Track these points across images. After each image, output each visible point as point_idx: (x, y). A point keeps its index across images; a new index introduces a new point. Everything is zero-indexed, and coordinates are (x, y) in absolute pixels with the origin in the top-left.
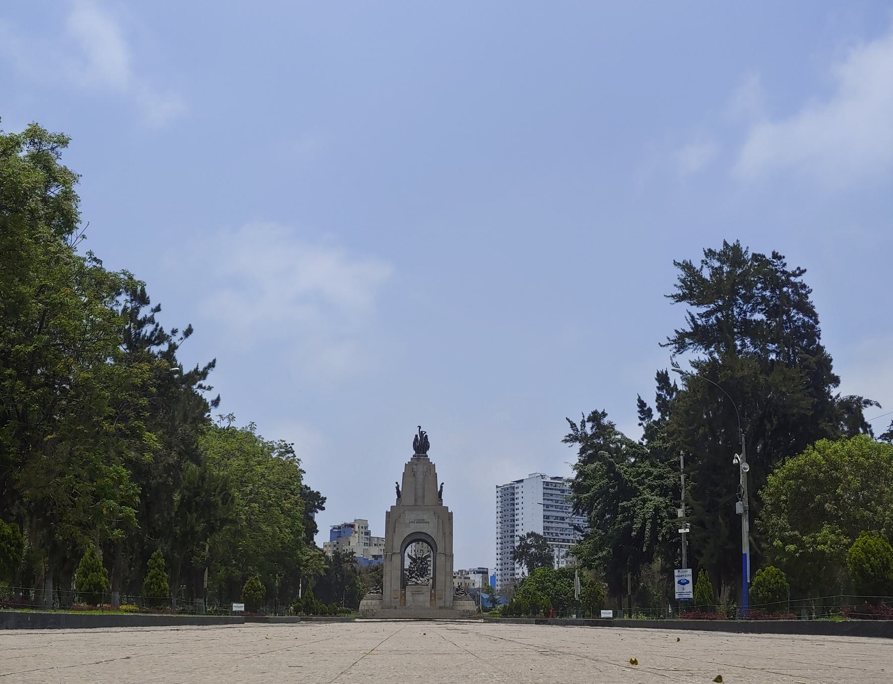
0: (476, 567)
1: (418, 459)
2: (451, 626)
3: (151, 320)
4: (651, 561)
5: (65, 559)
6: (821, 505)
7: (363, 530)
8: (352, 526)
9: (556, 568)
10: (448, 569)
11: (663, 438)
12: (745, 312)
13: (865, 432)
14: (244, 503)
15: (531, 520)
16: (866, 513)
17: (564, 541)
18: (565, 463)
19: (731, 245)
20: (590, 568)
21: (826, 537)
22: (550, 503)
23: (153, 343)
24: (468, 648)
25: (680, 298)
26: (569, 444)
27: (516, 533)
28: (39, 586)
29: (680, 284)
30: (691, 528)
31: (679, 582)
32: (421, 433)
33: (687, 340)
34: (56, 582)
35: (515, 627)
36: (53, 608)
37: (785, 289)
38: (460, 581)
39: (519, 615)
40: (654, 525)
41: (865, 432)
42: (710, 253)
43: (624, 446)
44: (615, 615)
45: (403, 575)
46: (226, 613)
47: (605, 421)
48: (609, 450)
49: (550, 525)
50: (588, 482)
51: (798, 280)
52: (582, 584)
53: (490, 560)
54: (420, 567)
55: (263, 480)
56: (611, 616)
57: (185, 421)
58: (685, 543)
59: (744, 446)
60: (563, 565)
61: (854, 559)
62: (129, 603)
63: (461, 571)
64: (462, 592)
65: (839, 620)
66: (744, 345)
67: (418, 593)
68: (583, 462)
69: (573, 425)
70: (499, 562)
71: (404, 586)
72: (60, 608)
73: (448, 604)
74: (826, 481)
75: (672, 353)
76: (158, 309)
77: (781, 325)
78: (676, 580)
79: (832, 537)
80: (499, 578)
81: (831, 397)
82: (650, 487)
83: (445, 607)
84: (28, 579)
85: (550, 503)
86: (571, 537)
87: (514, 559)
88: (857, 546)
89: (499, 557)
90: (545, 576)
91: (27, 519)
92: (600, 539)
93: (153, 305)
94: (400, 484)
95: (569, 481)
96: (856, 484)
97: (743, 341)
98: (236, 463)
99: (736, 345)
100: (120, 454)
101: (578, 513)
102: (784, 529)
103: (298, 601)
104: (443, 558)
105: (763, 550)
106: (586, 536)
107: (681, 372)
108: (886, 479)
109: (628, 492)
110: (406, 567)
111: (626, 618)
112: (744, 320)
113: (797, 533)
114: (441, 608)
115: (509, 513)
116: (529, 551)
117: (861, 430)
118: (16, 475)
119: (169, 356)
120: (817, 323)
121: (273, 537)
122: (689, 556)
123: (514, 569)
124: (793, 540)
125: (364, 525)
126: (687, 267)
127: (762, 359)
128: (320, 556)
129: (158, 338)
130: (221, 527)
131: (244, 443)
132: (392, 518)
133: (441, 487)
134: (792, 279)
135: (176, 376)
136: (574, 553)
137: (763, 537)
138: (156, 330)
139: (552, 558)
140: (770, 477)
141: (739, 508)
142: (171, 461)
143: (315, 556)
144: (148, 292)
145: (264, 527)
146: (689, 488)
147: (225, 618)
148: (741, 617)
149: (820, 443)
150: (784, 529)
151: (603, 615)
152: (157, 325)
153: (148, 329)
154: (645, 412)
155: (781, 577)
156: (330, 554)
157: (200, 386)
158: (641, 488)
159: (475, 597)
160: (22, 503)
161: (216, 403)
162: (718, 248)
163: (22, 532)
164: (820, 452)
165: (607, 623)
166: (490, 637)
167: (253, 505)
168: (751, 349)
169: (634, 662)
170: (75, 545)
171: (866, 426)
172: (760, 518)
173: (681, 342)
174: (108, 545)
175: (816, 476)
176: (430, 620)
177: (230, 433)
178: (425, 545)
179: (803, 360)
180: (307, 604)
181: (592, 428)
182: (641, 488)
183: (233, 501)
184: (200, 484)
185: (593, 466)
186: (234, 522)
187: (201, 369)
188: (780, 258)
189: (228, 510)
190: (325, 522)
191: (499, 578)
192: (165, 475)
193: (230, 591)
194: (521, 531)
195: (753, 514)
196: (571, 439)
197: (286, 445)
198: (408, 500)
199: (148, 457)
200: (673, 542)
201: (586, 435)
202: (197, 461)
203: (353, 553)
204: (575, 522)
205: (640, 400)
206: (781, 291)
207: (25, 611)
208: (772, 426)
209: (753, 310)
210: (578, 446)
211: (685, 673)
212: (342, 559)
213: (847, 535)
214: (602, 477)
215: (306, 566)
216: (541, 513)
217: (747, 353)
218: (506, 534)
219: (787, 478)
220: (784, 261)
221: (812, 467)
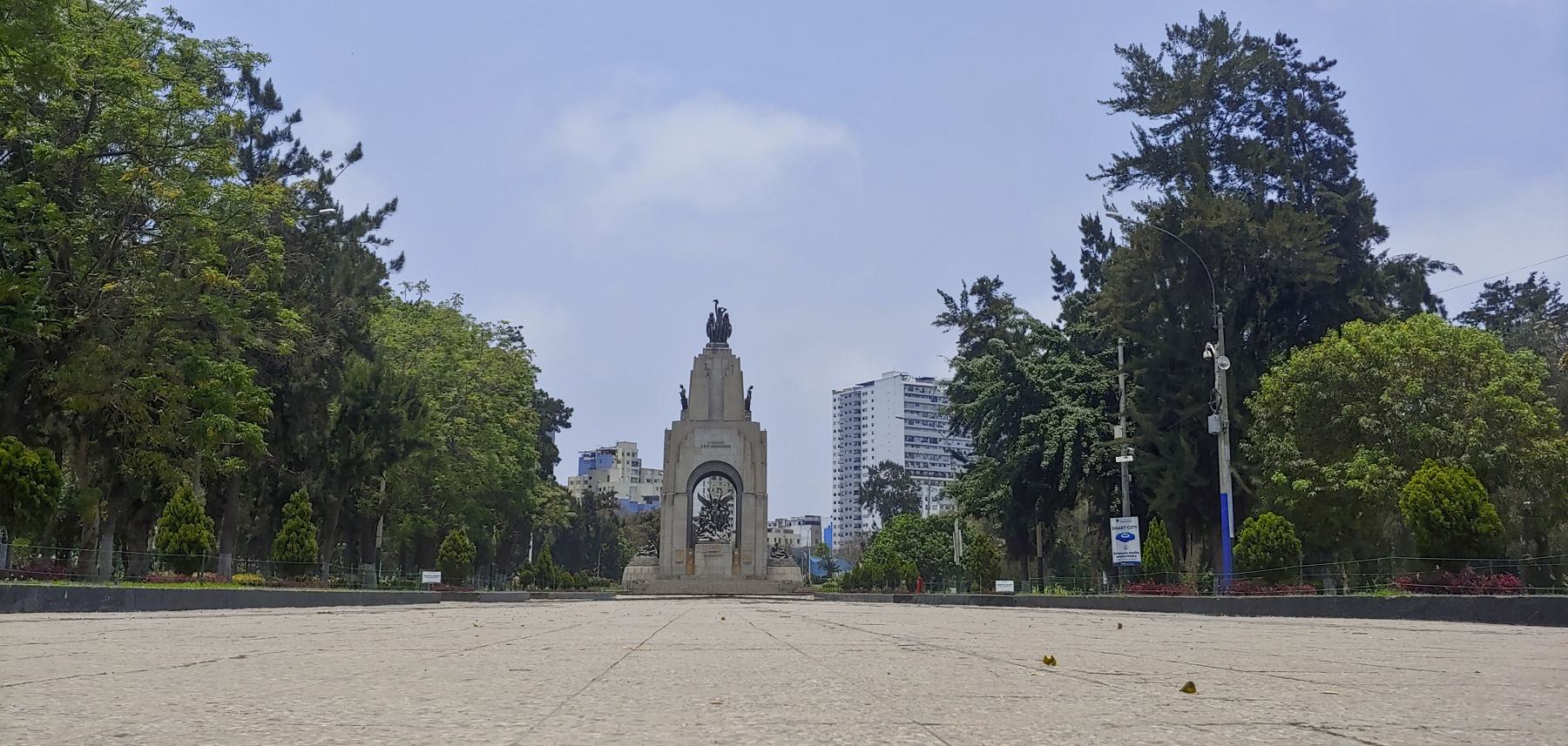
0: (802, 515)
2: (764, 605)
3: (287, 136)
4: (1072, 505)
5: (137, 505)
6: (1353, 418)
7: (630, 458)
8: (613, 452)
9: (925, 516)
10: (760, 518)
11: (1091, 319)
12: (1229, 126)
13: (1432, 309)
14: (444, 417)
15: (886, 443)
16: (1433, 430)
17: (936, 474)
18: (939, 358)
19: (1210, 18)
20: (978, 515)
21: (1361, 469)
22: (915, 416)
24: (790, 640)
25: (1123, 106)
26: (943, 328)
27: (863, 463)
28: (89, 545)
29: (1126, 82)
30: (1136, 455)
31: (1119, 537)
32: (719, 311)
34: (121, 539)
35: (864, 607)
36: (112, 579)
37: (1297, 92)
38: (778, 536)
39: (869, 589)
41: (1432, 309)
42: (1177, 32)
43: (1029, 331)
44: (1018, 588)
45: (690, 527)
46: (411, 586)
47: (999, 293)
48: (1004, 336)
49: (914, 450)
50: (974, 385)
51: (1320, 77)
52: (966, 540)
54: (716, 514)
55: (474, 382)
56: (1012, 589)
57: (348, 292)
58: (1126, 478)
59: (1221, 331)
60: (935, 512)
61: (1414, 501)
62: (248, 570)
63: (780, 521)
64: (779, 553)
65: (1390, 595)
66: (1225, 178)
67: (713, 554)
68: (965, 355)
69: (948, 300)
70: (838, 506)
71: (692, 544)
72: (125, 580)
73: (759, 573)
74: (1366, 384)
75: (1107, 189)
76: (296, 118)
77: (1289, 148)
78: (1114, 534)
79: (1374, 468)
80: (837, 531)
81: (1371, 257)
82: (1069, 392)
84: (69, 533)
85: (915, 416)
86: (948, 469)
87: (861, 502)
89: (838, 498)
90: (908, 528)
91: (70, 440)
92: (993, 472)
93: (288, 111)
94: (687, 388)
95: (943, 383)
96: (1416, 387)
97: (1224, 170)
98: (429, 356)
99: (1211, 178)
100: (239, 341)
101: (957, 432)
102: (1290, 457)
103: (528, 567)
104: (752, 500)
105: (1254, 488)
106: (971, 467)
107: (1119, 219)
108: (1469, 380)
110: (696, 514)
111: (1035, 592)
112: (1228, 138)
113: (1311, 461)
114: (748, 577)
115: (853, 432)
116: (886, 491)
117: (1424, 307)
118: (49, 374)
119: (319, 194)
120: (1352, 144)
121: (489, 468)
122: (1132, 498)
123: (860, 518)
124: (1305, 472)
126: (1136, 55)
127: (1253, 199)
128: (563, 498)
129: (298, 163)
130: (405, 454)
131: (443, 326)
132: (674, 441)
134: (1311, 75)
136: (954, 494)
137: (1254, 468)
138: (295, 151)
139: (919, 500)
140: (1264, 378)
141: (1214, 424)
142: (324, 353)
144: (279, 92)
145: (475, 454)
146: (1132, 394)
147: (406, 592)
148: (1222, 591)
149: (1351, 327)
150: (1290, 457)
151: (998, 589)
152: (297, 144)
153: (281, 150)
154: (1062, 278)
155: (1286, 529)
156: (578, 495)
157: (371, 239)
158: (1055, 394)
159: (800, 561)
160: (60, 417)
161: (398, 264)
162: (1191, 23)
163: (59, 460)
164: (1350, 341)
165: (1006, 601)
166: (823, 623)
168: (1238, 183)
169: (1050, 661)
170: (156, 482)
171: (1433, 302)
172: (1248, 440)
173: (1121, 173)
174: (216, 485)
175: (1344, 377)
176: (731, 596)
177: (421, 311)
178: (725, 480)
180: (542, 572)
181: (979, 303)
182: (1055, 394)
183: (424, 413)
184: (373, 387)
185: (981, 361)
186: (424, 446)
187: (372, 214)
188: (1289, 43)
189: (418, 428)
190: (570, 445)
191: (837, 531)
192: (315, 375)
193: (418, 553)
194: (871, 460)
195: (1236, 434)
196: (947, 320)
197: (510, 329)
198: (699, 412)
199: (286, 346)
200: (1107, 475)
201: (970, 314)
202: (368, 353)
203: (613, 493)
204: (954, 445)
205: (1054, 260)
206: (1290, 94)
207: (59, 584)
208: (1268, 300)
209: (1243, 123)
210: (957, 331)
211: (1134, 679)
213: (1398, 465)
214: (994, 378)
215: (540, 514)
216: (902, 433)
217: (1232, 190)
218: (848, 464)
219: (1293, 379)
220: (1297, 46)
221: (1336, 362)
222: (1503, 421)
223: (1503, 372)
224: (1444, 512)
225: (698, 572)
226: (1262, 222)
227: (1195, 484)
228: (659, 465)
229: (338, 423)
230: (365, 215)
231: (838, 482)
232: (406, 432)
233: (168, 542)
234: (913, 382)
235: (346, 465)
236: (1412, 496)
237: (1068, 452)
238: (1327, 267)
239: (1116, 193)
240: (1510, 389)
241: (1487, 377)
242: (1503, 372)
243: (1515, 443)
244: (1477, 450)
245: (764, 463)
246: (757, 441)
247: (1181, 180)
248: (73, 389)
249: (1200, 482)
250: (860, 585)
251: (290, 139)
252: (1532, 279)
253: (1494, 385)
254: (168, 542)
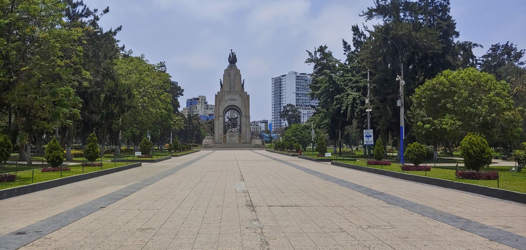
0: (261, 120)
1: (231, 67)
6: (445, 104)
8: (198, 99)
15: (290, 98)
17: (306, 106)
22: (299, 86)
23: (84, 16)
26: (308, 64)
27: (282, 105)
30: (373, 109)
31: (366, 136)
32: (232, 53)
33: (374, 13)
40: (353, 107)
47: (327, 51)
49: (299, 98)
53: (269, 117)
54: (233, 123)
58: (369, 117)
61: (464, 147)
63: (254, 122)
64: (256, 134)
66: (405, 15)
67: (233, 136)
69: (310, 54)
70: (273, 117)
71: (225, 132)
78: (365, 135)
80: (273, 125)
81: (454, 43)
82: (351, 87)
83: (246, 143)
85: (299, 86)
88: (465, 141)
89: (273, 114)
90: (297, 129)
92: (325, 114)
98: (134, 77)
99: (400, 16)
102: (424, 116)
104: (245, 118)
105: (412, 123)
109: (339, 90)
113: (431, 118)
116: (289, 114)
119: (94, 23)
120: (449, 4)
121: (156, 114)
122: (371, 122)
124: (428, 122)
125: (204, 98)
132: (218, 97)
135: (99, 34)
138: (85, 9)
139: (300, 116)
141: (399, 103)
143: (178, 119)
146: (372, 87)
149: (445, 72)
150: (424, 116)
152: (85, 6)
153: (80, 9)
158: (346, 88)
159: (261, 137)
167: (145, 98)
168: (409, 18)
173: (370, 14)
175: (442, 90)
179: (438, 24)
181: (320, 55)
182: (346, 88)
184: (115, 88)
187: (113, 31)
191: (273, 125)
194: (285, 103)
195: (407, 105)
196: (309, 61)
198: (226, 89)
201: (317, 59)
202: (113, 79)
208: (418, 57)
210: (313, 64)
212: (192, 118)
217: (407, 20)
218: (277, 103)
219: (426, 89)
222: (495, 106)
223: (496, 88)
224: (474, 151)
225: (227, 142)
226: (417, 32)
227: (392, 121)
228: (213, 103)
229: (104, 100)
230: (110, 31)
232: (127, 103)
233: (49, 157)
234: (299, 75)
235: (108, 114)
236: (463, 145)
237: (350, 108)
238: (438, 47)
239: (368, 21)
240: (498, 94)
241: (490, 90)
242: (496, 88)
243: (498, 114)
244: (485, 116)
245: (249, 106)
246: (246, 98)
247: (390, 17)
248: (14, 100)
249: (393, 120)
250: (280, 148)
251: (83, 5)
252: (508, 43)
253: (492, 94)
254: (49, 157)
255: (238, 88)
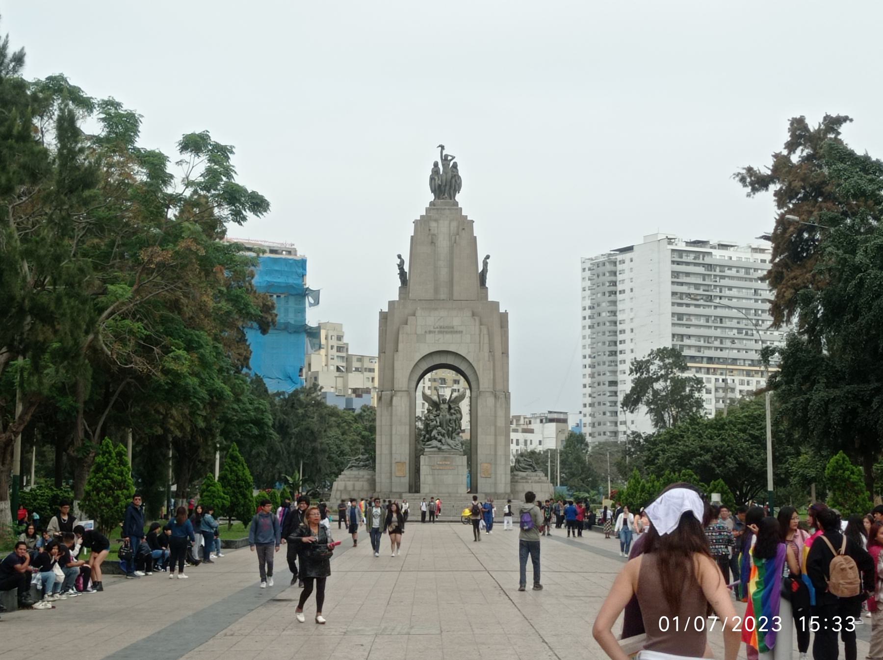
0: (543, 410)
7: (334, 342)
17: (710, 360)
32: (445, 159)
85: (684, 289)
104: (491, 401)
133: (485, 264)
162: (746, 166)
231: (588, 371)
234: (682, 246)
245: (505, 353)
255: (465, 285)
